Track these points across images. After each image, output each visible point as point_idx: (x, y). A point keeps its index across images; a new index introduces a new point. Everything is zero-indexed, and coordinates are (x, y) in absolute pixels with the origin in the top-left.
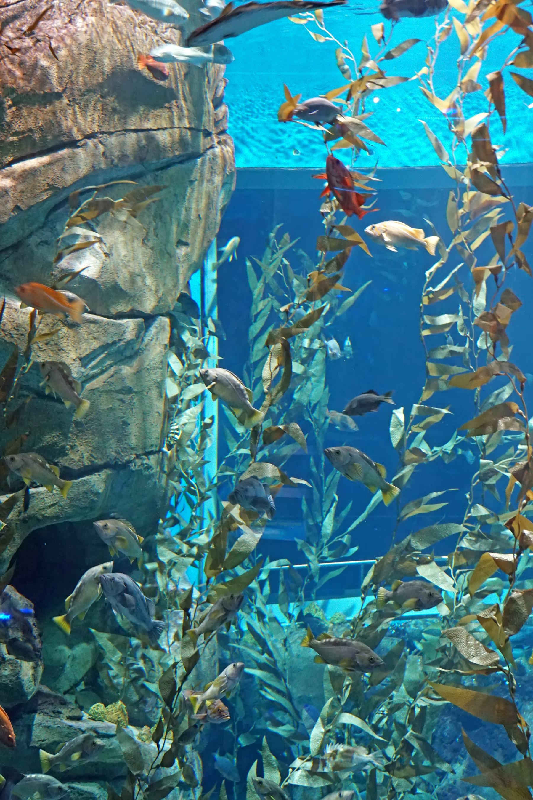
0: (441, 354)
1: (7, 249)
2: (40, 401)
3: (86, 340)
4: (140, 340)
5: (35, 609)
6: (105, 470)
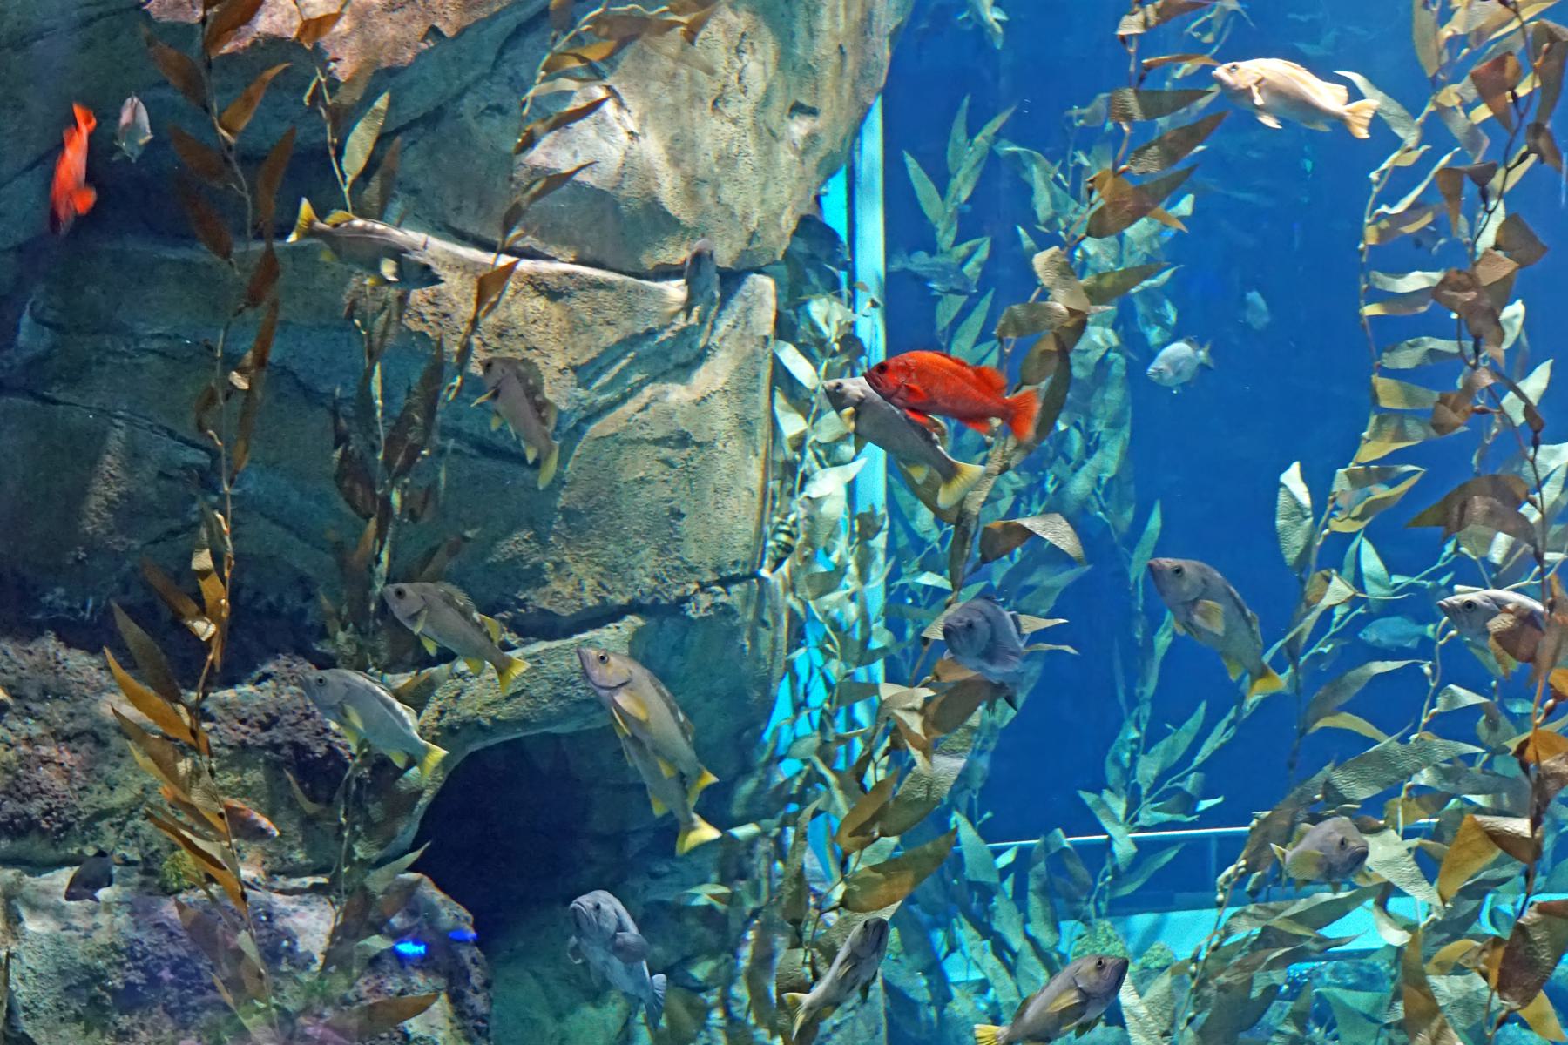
0: (1406, 358)
4: (708, 327)
5: (476, 926)
6: (630, 618)
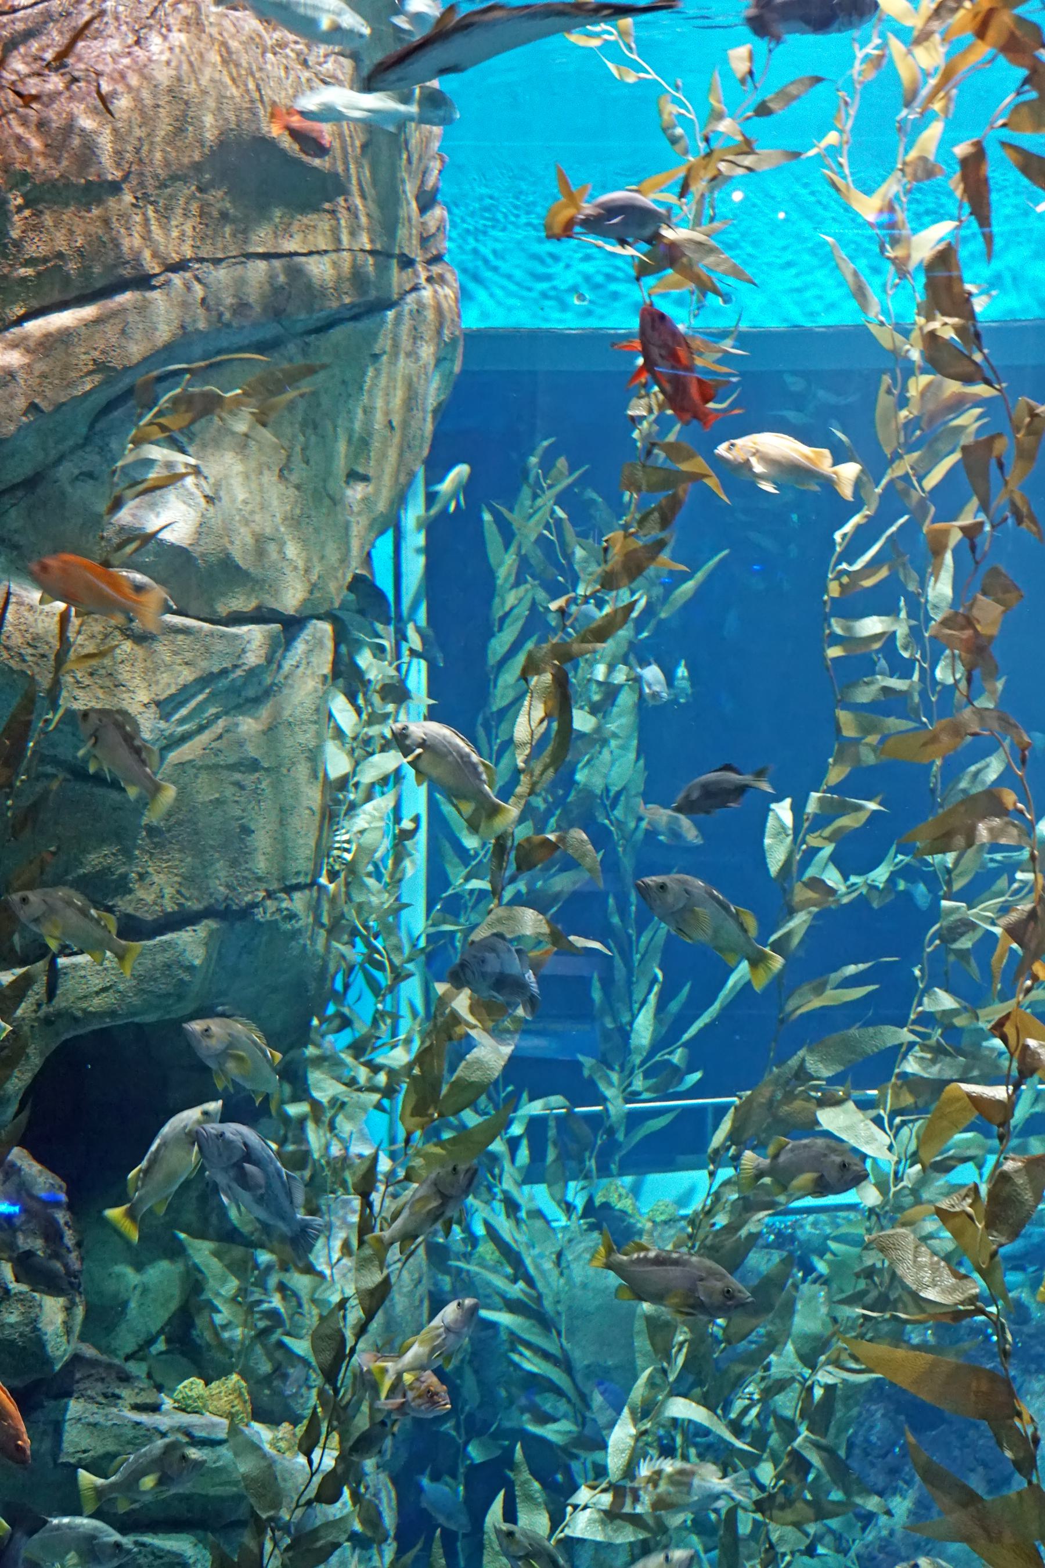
0: (865, 694)
1: (13, 488)
2: (79, 787)
3: (168, 667)
4: (274, 666)
5: (68, 1193)
6: (205, 922)
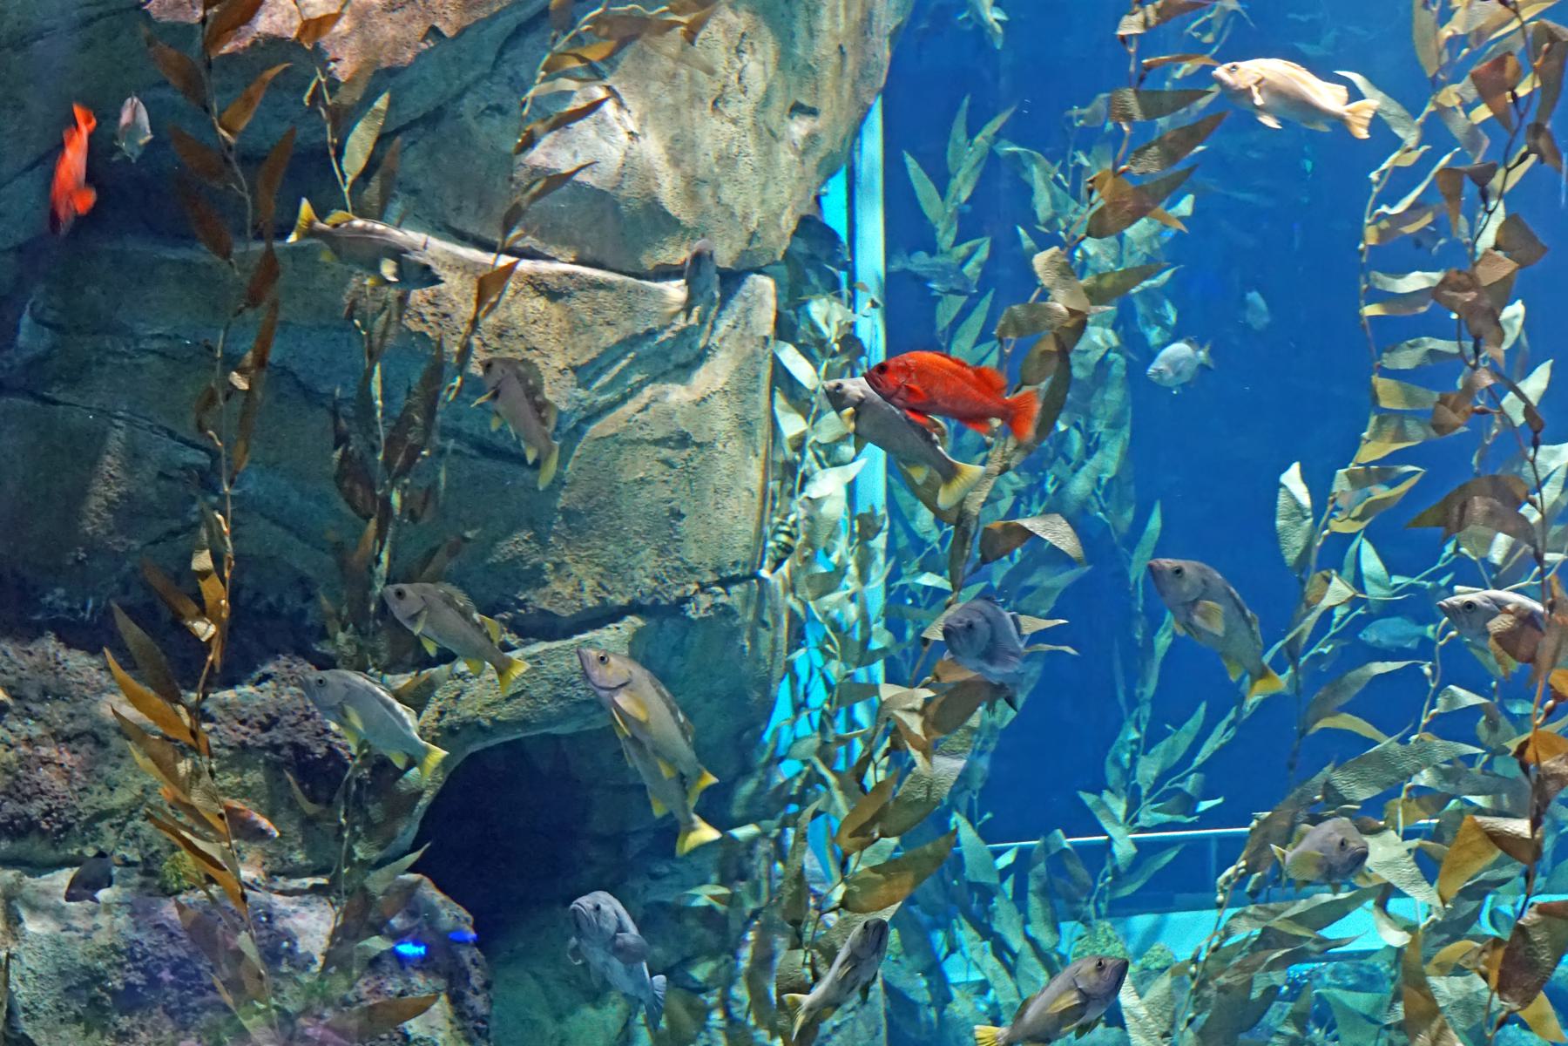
0: (1406, 359)
4: (708, 327)
5: (476, 927)
6: (630, 618)
